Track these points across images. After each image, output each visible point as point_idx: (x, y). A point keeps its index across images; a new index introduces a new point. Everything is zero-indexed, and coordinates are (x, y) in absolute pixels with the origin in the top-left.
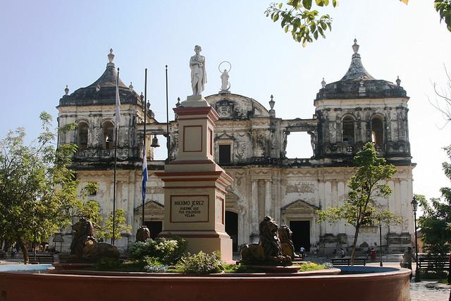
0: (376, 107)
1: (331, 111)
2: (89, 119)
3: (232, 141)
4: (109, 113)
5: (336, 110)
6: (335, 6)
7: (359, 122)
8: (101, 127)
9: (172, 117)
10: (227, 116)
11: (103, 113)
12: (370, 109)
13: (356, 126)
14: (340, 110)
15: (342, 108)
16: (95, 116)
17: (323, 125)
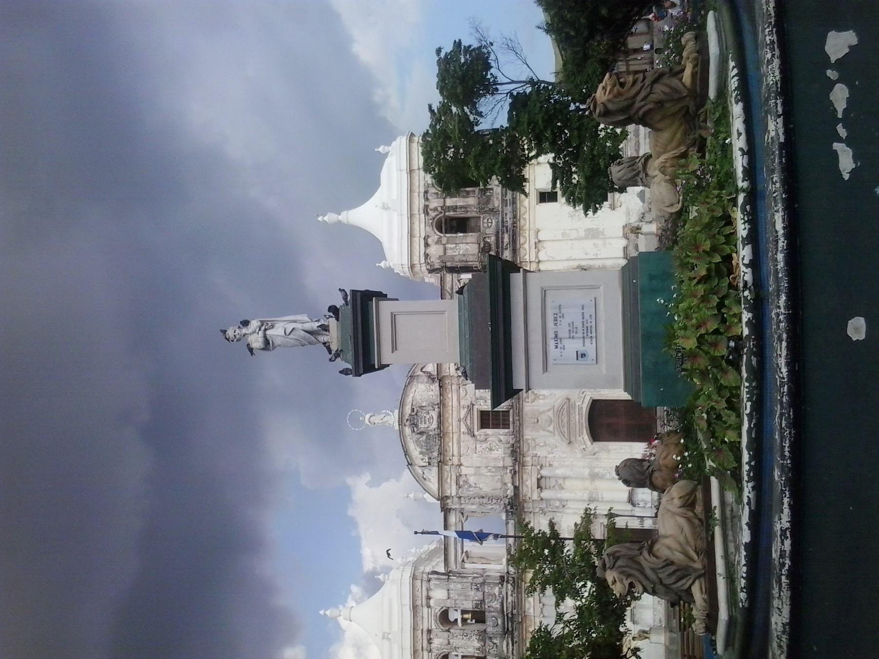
0: (422, 183)
1: (428, 251)
2: (435, 652)
3: (476, 407)
4: (425, 616)
5: (427, 245)
6: (341, 372)
7: (445, 208)
8: (448, 631)
9: (609, 195)
10: (435, 417)
11: (425, 629)
12: (426, 192)
13: (451, 214)
14: (426, 239)
15: (423, 235)
16: (430, 641)
17: (449, 264)
